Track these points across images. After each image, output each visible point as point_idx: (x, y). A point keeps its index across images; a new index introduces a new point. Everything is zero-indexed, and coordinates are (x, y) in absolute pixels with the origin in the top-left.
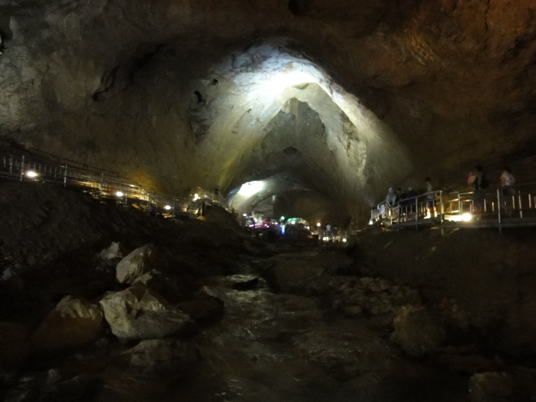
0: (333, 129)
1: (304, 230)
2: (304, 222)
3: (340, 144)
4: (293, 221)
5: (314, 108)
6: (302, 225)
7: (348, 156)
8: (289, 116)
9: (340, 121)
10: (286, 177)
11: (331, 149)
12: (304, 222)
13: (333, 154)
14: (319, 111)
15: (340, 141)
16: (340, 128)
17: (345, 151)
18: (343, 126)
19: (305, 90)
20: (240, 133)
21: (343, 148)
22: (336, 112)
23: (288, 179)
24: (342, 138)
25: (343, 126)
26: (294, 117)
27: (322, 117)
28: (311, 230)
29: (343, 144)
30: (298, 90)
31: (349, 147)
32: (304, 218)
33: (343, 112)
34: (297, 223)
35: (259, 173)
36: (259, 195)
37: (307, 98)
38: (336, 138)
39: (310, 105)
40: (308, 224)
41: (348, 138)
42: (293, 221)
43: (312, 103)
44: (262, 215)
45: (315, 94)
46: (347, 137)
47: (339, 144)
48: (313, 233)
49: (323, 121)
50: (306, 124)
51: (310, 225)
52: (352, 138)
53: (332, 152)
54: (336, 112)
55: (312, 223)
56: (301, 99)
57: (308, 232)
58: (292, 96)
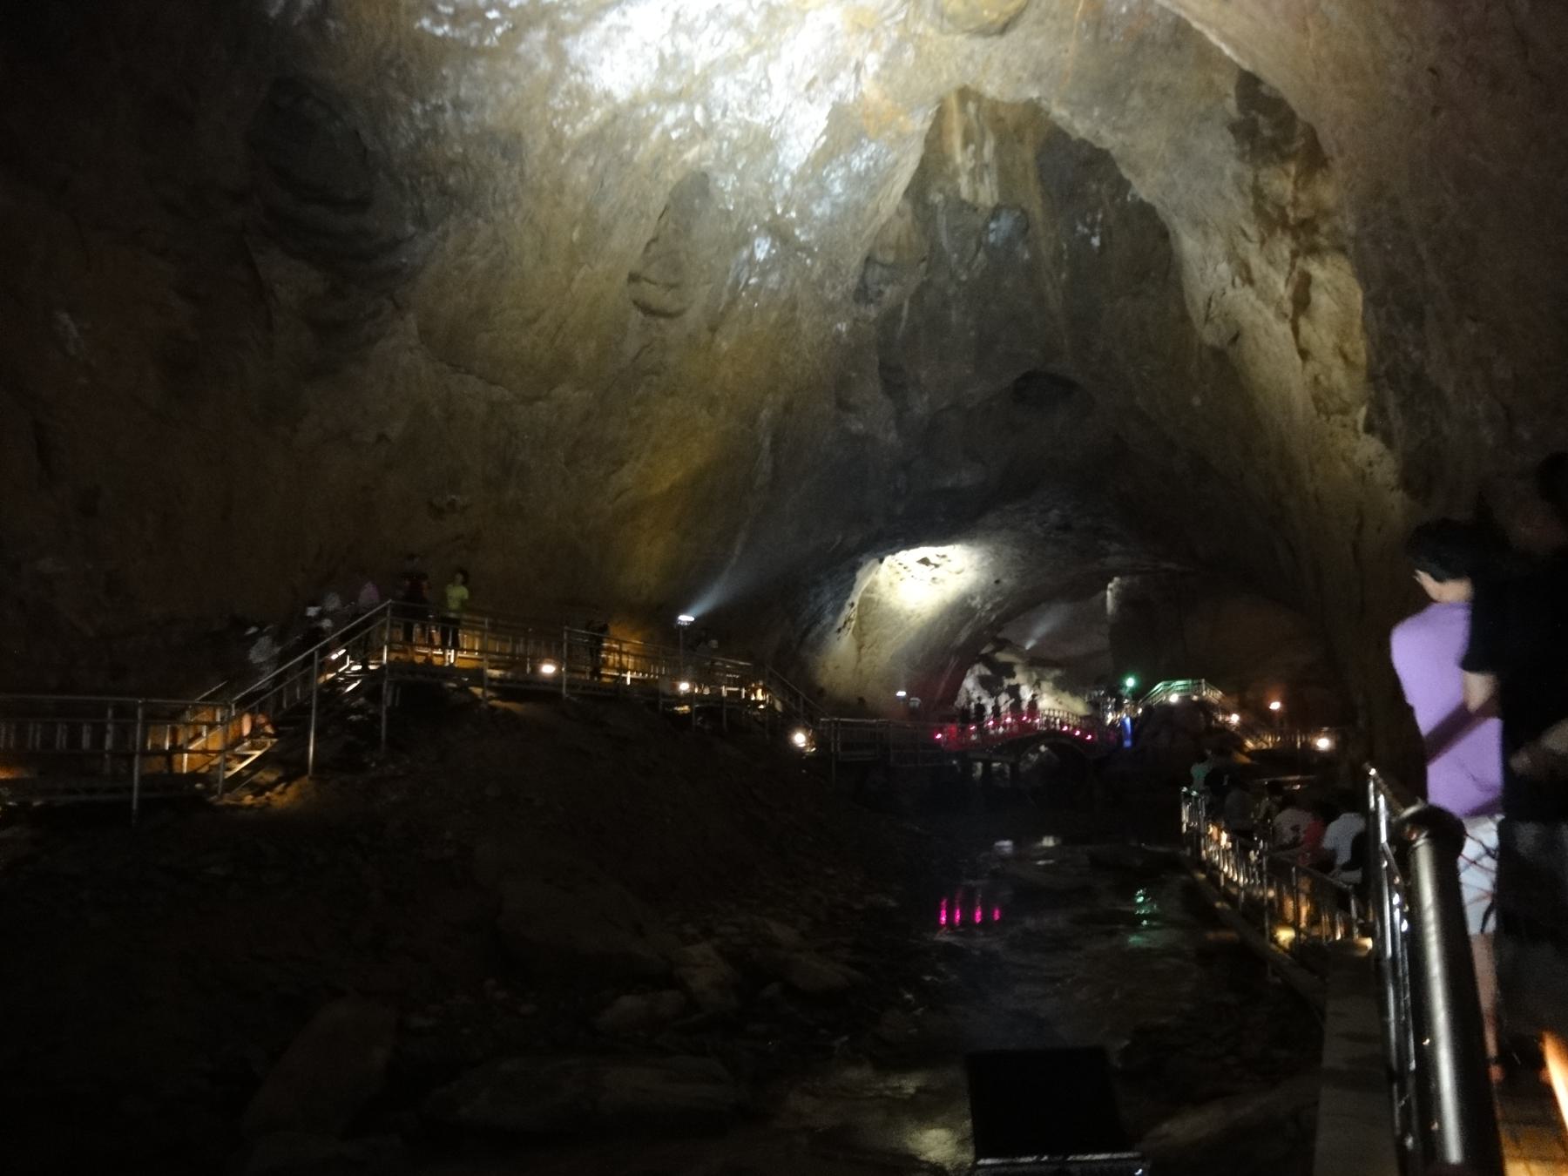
0: (1198, 223)
1: (1210, 730)
2: (1214, 695)
3: (1250, 293)
4: (1172, 693)
5: (1081, 128)
6: (1205, 707)
7: (1304, 354)
8: (1005, 224)
9: (1232, 166)
10: (1054, 515)
11: (1209, 336)
12: (1214, 695)
13: (1226, 364)
14: (1110, 140)
15: (1249, 281)
16: (1240, 209)
17: (1284, 328)
18: (1257, 191)
19: (1017, 34)
20: (694, 316)
21: (1270, 314)
22: (1204, 118)
23: (1066, 527)
24: (1256, 262)
25: (1257, 191)
26: (1024, 227)
27: (1133, 167)
28: (1246, 729)
29: (1263, 295)
30: (978, 44)
31: (1303, 301)
32: (1214, 683)
33: (1178, 18)
34: (1186, 699)
35: (900, 509)
36: (977, 602)
37: (1037, 78)
38: (1223, 268)
39: (1059, 113)
40: (1231, 702)
41: (1295, 254)
42: (1172, 693)
43: (1065, 102)
44: (1057, 672)
45: (1072, 45)
46: (1284, 247)
47: (1243, 301)
48: (1250, 744)
49: (1145, 188)
50: (1086, 239)
51: (1240, 709)
52: (1313, 250)
53: (1219, 354)
54: (1204, 118)
55: (1250, 696)
56: (993, 88)
57: (1231, 740)
58: (949, 77)
